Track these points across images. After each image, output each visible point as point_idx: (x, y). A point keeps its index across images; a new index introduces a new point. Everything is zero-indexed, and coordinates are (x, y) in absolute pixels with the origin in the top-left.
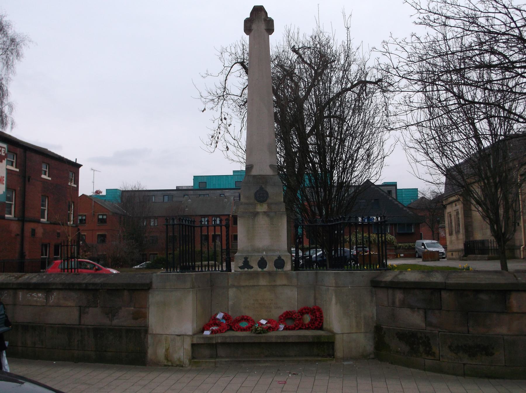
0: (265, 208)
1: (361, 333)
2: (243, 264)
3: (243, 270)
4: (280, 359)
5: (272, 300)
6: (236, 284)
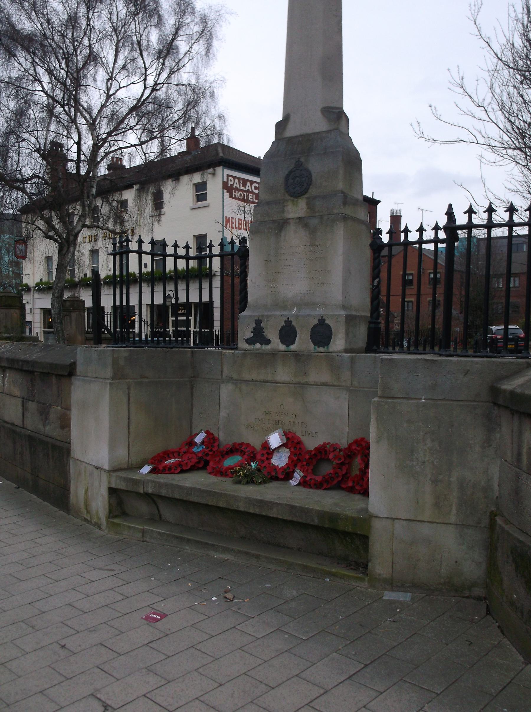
0: (302, 209)
1: (447, 524)
2: (252, 335)
3: (252, 346)
4: (253, 552)
5: (297, 416)
6: (235, 376)
